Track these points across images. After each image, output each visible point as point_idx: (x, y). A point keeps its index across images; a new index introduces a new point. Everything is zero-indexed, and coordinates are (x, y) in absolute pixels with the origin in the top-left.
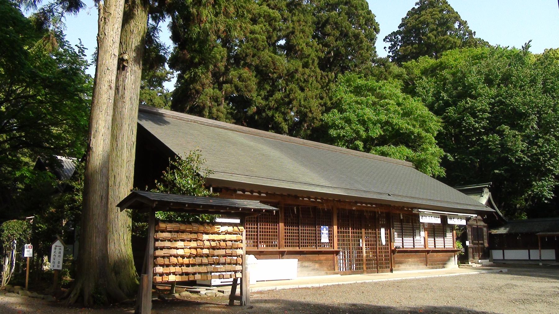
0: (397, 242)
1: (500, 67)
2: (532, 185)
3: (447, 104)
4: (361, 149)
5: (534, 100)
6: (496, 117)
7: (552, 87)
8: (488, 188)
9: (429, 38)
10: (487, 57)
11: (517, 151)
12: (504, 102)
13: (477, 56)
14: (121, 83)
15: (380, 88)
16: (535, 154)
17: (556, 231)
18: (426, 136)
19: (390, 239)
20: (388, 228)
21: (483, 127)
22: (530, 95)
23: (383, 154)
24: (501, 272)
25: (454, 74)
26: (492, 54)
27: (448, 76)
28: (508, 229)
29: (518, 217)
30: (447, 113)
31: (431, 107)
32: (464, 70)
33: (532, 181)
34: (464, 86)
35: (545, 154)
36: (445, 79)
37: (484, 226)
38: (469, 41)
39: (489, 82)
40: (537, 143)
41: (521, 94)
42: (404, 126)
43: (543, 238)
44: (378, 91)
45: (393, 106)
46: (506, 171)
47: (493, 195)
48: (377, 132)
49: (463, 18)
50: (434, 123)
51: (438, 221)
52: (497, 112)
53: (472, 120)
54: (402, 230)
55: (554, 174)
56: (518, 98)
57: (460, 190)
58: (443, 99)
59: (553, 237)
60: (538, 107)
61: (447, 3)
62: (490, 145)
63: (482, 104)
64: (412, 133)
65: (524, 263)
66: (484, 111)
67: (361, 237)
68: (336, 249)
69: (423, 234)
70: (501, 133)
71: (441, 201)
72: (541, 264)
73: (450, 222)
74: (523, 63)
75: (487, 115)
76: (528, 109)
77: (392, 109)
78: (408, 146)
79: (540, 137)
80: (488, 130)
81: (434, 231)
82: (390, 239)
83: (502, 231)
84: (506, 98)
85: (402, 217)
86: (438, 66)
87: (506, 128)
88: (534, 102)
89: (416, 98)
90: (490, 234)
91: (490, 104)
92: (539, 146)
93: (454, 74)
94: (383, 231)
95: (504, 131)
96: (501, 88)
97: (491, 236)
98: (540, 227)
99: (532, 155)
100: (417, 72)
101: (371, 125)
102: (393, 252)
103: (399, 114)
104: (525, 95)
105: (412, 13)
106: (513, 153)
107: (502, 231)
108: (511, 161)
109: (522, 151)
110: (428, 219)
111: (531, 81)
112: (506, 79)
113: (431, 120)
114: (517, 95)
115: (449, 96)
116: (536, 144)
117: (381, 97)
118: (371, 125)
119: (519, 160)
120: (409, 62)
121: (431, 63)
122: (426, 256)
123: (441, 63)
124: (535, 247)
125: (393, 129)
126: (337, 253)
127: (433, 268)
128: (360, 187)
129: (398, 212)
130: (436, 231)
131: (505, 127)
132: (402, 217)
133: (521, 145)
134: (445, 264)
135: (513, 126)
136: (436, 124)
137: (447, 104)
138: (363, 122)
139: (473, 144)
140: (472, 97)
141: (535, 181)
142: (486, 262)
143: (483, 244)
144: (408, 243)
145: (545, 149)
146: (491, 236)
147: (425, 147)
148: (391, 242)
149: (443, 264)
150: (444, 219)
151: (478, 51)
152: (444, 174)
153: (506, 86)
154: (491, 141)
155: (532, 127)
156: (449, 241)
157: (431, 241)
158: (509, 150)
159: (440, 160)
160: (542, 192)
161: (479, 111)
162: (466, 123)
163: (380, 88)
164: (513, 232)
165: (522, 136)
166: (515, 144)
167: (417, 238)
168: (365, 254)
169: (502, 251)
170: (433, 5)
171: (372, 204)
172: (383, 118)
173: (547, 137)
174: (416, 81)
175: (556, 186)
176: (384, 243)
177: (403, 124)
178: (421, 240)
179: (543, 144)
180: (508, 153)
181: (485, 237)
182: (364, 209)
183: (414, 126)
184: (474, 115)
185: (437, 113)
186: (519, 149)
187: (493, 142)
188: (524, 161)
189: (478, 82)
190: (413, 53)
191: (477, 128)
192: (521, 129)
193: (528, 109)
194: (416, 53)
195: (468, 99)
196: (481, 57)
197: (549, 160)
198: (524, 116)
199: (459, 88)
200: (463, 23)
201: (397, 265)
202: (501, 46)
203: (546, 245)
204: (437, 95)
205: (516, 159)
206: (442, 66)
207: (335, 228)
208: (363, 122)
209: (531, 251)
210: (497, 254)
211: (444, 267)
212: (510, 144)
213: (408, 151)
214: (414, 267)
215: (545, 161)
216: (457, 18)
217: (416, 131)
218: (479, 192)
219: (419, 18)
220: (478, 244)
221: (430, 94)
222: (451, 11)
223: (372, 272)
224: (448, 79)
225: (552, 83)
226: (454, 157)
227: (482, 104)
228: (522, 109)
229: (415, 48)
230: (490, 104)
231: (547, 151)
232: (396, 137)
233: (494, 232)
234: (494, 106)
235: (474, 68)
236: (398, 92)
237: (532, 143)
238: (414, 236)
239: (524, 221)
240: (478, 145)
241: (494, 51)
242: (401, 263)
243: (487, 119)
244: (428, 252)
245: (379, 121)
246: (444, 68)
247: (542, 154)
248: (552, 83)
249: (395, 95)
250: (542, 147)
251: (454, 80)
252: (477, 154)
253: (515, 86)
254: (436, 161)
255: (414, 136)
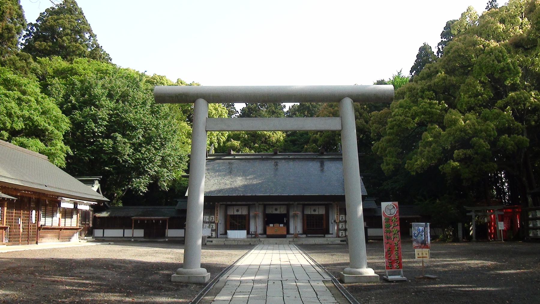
0: (42, 222)
1: (120, 85)
2: (132, 182)
3: (74, 107)
4: (6, 138)
5: (143, 118)
6: (112, 126)
7: (157, 111)
8: (98, 180)
9: (63, 41)
10: (110, 74)
11: (124, 155)
12: (120, 115)
13: (102, 71)
14: (242, 243)
15: (25, 85)
16: (138, 159)
17: (147, 216)
18: (57, 134)
19: (38, 219)
20: (37, 210)
21: (101, 132)
22: (140, 113)
23: (22, 145)
24: (110, 244)
25: (82, 81)
26: (115, 73)
27: (77, 83)
28: (109, 213)
29: (115, 204)
30: (73, 115)
31: (61, 106)
32: (93, 81)
33: (132, 178)
34: (90, 95)
35: (145, 160)
36: (74, 84)
37: (91, 210)
38: (96, 54)
39: (110, 96)
40: (140, 151)
41: (134, 111)
42: (42, 124)
43: (136, 221)
44: (23, 88)
45: (34, 105)
46: (114, 168)
47: (101, 186)
48: (20, 125)
49: (95, 32)
50: (65, 123)
51: (71, 206)
52: (114, 121)
53: (93, 125)
54: (46, 212)
55: (149, 174)
56: (131, 115)
57: (80, 180)
58: (71, 102)
59: (144, 220)
60: (145, 124)
61: (83, 14)
62: (104, 147)
63: (103, 114)
64: (47, 130)
65: (119, 239)
66: (103, 119)
67: (20, 217)
68: (4, 226)
69: (59, 215)
70: (114, 139)
71: (63, 190)
72: (133, 240)
73: (79, 207)
74: (138, 87)
75: (105, 123)
76: (138, 124)
77: (34, 107)
78: (42, 141)
79: (144, 147)
80: (107, 136)
81: (65, 214)
82: (38, 219)
83: (104, 214)
84: (122, 112)
85: (47, 202)
86: (69, 71)
87: (119, 137)
88: (142, 120)
89: (52, 99)
90: (95, 216)
91: (109, 114)
92: (142, 153)
93: (82, 81)
94: (34, 212)
95: (116, 138)
96: (119, 104)
97: (95, 218)
98: (134, 213)
99: (136, 159)
100: (50, 71)
101: (16, 119)
102: (39, 229)
103: (39, 112)
104: (136, 112)
105: (51, 12)
106: (122, 155)
107: (104, 214)
108: (119, 161)
109: (128, 155)
110: (67, 204)
111: (143, 103)
112: (124, 97)
113: (63, 121)
114: (131, 112)
115: (77, 100)
116: (140, 151)
117: (24, 93)
118: (16, 119)
119: (126, 161)
120: (43, 59)
121: (63, 66)
122: (58, 231)
123: (72, 69)
124: (129, 227)
125: (33, 124)
126: (5, 228)
127: (63, 241)
128: (28, 179)
129: (45, 198)
130: (67, 214)
131: (117, 134)
132: (47, 202)
133: (129, 150)
134: (71, 238)
135: (124, 135)
136: (66, 125)
137: (74, 107)
138: (10, 115)
139: (91, 144)
140: (96, 106)
141: (135, 178)
142: (90, 238)
143: (89, 224)
144: (47, 222)
145: (146, 156)
146: (95, 218)
147: (54, 142)
148: (38, 221)
149: (69, 238)
150: (75, 204)
151: (104, 66)
152: (64, 166)
153: (123, 102)
154: (106, 144)
155: (139, 138)
156: (73, 222)
157: (63, 220)
158: (118, 153)
159: (65, 155)
160: (139, 187)
161: (100, 119)
162: (88, 127)
163: (25, 85)
164: (113, 215)
165: (130, 143)
166: (124, 149)
167: (54, 218)
168: (21, 230)
169: (102, 230)
170: (71, 12)
171: (28, 191)
172: (27, 114)
173: (149, 147)
174: (48, 78)
175: (150, 183)
176: (34, 222)
177: (42, 121)
178: (56, 221)
179: (145, 152)
180: (117, 155)
181: (91, 219)
182: (25, 195)
183: (49, 124)
184: (95, 122)
185: (67, 112)
186: (127, 153)
187: (107, 145)
188: (129, 163)
189: (102, 96)
190: (47, 49)
191: (96, 132)
192: (130, 138)
193: (138, 124)
194: (50, 51)
195: (93, 107)
196: (106, 72)
197: (148, 164)
198: (134, 129)
199: (86, 96)
200: (92, 36)
201: (40, 239)
202: (121, 68)
203: (137, 227)
204: (66, 97)
205: (123, 160)
206: (73, 72)
207: (6, 208)
208: (10, 115)
209: (125, 230)
210: (98, 233)
211: (69, 241)
212: (120, 149)
213: (41, 145)
214: (51, 240)
215: (145, 165)
216: (90, 31)
217: (51, 128)
218: (92, 183)
219: (57, 19)
220: (85, 224)
221: (61, 96)
222: (85, 23)
223: (24, 244)
224: (76, 85)
225: (158, 107)
226: (74, 152)
227: (103, 114)
228: (134, 123)
229: (49, 46)
230: (109, 114)
231: (147, 157)
232: (34, 131)
233: (98, 215)
234: (112, 117)
235: (100, 83)
236: (38, 90)
237: (136, 150)
238: (52, 217)
239: (120, 208)
240: (95, 145)
241: (116, 70)
242: (43, 237)
243: (105, 126)
244: (61, 229)
245: (23, 116)
246: (76, 74)
247: (144, 159)
248: (158, 107)
249: (36, 94)
250: (144, 154)
251: (82, 87)
252: (92, 152)
253: (130, 105)
254: (63, 156)
255: (49, 133)
